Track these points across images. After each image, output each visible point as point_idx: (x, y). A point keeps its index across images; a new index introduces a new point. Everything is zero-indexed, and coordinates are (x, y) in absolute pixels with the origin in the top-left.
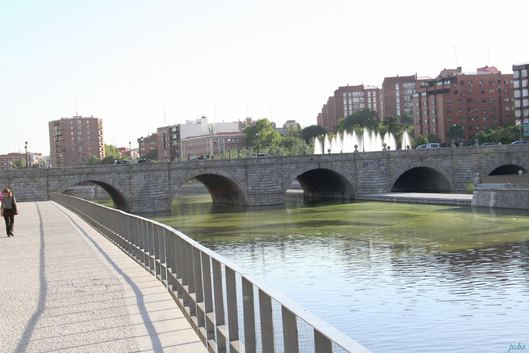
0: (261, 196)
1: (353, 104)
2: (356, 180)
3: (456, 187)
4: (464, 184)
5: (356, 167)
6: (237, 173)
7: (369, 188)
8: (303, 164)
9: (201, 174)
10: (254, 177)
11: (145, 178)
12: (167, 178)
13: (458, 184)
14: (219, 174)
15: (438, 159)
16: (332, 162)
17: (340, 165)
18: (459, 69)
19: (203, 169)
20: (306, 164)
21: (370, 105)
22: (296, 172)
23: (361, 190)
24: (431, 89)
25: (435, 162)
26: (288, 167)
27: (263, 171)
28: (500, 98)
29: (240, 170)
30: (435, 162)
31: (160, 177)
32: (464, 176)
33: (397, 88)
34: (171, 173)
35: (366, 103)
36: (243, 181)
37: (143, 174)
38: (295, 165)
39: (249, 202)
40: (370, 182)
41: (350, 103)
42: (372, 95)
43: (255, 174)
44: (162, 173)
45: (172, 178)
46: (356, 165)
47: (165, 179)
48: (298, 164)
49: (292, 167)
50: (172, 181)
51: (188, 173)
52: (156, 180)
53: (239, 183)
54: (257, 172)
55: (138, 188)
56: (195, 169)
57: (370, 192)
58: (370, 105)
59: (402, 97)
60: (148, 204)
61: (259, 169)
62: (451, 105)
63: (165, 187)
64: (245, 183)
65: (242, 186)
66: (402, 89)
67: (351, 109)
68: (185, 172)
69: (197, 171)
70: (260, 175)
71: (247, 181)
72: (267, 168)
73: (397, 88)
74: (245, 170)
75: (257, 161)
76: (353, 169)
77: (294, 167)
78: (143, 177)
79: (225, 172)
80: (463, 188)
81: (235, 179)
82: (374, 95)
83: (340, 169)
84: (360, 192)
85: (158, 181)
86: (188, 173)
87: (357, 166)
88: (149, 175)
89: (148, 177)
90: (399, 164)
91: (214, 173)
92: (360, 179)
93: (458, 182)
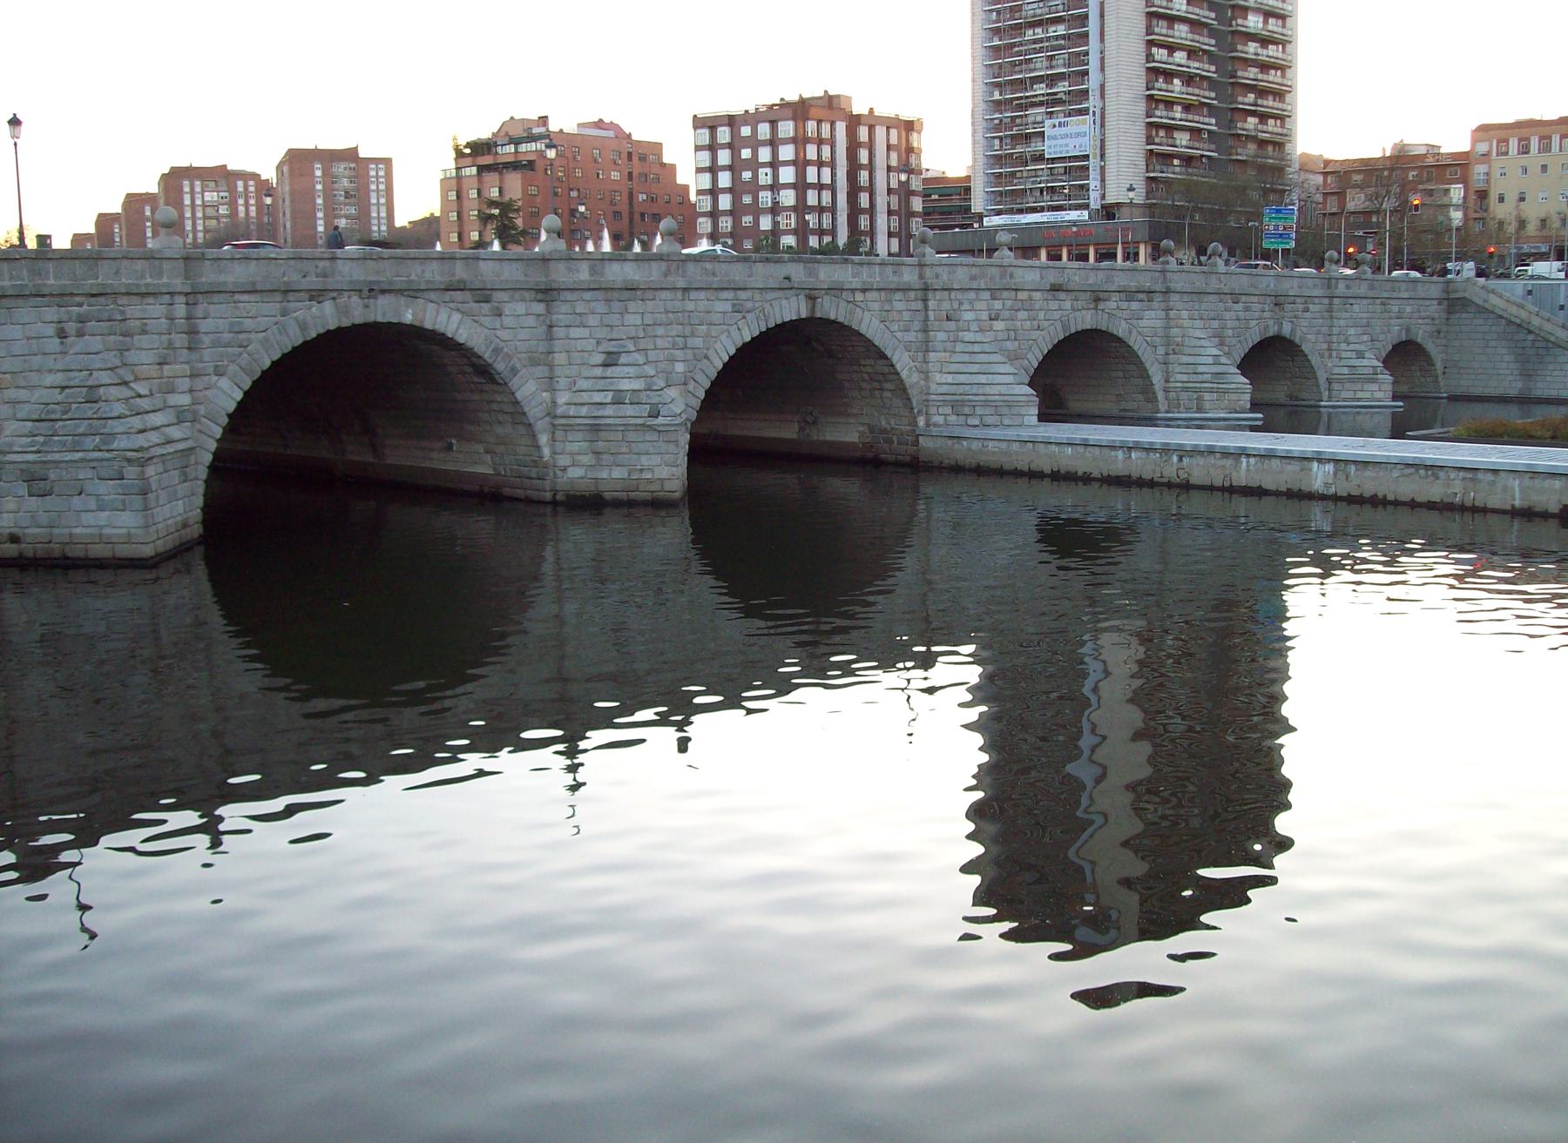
0: (631, 436)
1: (204, 206)
2: (926, 375)
3: (1175, 405)
4: (1207, 396)
5: (926, 319)
6: (508, 321)
7: (986, 404)
8: (757, 296)
9: (346, 323)
10: (580, 345)
11: (62, 335)
12: (180, 340)
13: (1184, 395)
14: (428, 325)
15: (1134, 305)
16: (853, 290)
17: (876, 306)
18: (544, 120)
19: (355, 298)
20: (770, 295)
21: (241, 209)
22: (735, 333)
23: (948, 410)
24: (486, 160)
25: (1125, 314)
26: (703, 305)
27: (614, 319)
28: (631, 195)
29: (521, 308)
30: (1125, 314)
31: (144, 332)
32: (1201, 369)
33: (318, 173)
34: (199, 311)
35: (233, 204)
36: (534, 362)
37: (51, 313)
38: (730, 295)
39: (563, 461)
40: (983, 379)
41: (199, 202)
42: (246, 187)
43: (584, 332)
44: (156, 309)
45: (207, 340)
46: (926, 309)
47: (170, 346)
48: (743, 295)
49: (720, 306)
50: (207, 354)
51: (284, 313)
52: (123, 350)
53: (514, 371)
54: (592, 321)
55: (23, 394)
56: (317, 295)
57: (989, 420)
58: (241, 209)
59: (328, 194)
60: (104, 488)
61: (601, 307)
62: (538, 199)
63: (172, 391)
64: (541, 371)
65: (528, 389)
66: (326, 172)
67: (199, 214)
68: (272, 307)
69: (328, 307)
70: (602, 333)
71: (551, 367)
72: (632, 306)
73: (318, 173)
74: (539, 308)
75: (593, 271)
76: (917, 325)
77: (728, 307)
78: (50, 330)
79: (456, 317)
80: (1199, 410)
81: (497, 351)
82: (252, 189)
83: (875, 322)
84: (939, 419)
85: (132, 357)
86: (284, 313)
87: (931, 314)
88: (82, 320)
89: (80, 334)
90: (1041, 315)
91: (408, 317)
92: (937, 367)
93: (1186, 389)
